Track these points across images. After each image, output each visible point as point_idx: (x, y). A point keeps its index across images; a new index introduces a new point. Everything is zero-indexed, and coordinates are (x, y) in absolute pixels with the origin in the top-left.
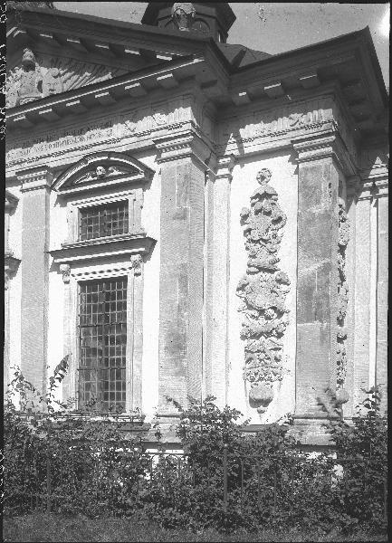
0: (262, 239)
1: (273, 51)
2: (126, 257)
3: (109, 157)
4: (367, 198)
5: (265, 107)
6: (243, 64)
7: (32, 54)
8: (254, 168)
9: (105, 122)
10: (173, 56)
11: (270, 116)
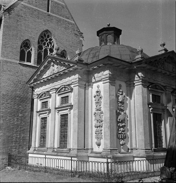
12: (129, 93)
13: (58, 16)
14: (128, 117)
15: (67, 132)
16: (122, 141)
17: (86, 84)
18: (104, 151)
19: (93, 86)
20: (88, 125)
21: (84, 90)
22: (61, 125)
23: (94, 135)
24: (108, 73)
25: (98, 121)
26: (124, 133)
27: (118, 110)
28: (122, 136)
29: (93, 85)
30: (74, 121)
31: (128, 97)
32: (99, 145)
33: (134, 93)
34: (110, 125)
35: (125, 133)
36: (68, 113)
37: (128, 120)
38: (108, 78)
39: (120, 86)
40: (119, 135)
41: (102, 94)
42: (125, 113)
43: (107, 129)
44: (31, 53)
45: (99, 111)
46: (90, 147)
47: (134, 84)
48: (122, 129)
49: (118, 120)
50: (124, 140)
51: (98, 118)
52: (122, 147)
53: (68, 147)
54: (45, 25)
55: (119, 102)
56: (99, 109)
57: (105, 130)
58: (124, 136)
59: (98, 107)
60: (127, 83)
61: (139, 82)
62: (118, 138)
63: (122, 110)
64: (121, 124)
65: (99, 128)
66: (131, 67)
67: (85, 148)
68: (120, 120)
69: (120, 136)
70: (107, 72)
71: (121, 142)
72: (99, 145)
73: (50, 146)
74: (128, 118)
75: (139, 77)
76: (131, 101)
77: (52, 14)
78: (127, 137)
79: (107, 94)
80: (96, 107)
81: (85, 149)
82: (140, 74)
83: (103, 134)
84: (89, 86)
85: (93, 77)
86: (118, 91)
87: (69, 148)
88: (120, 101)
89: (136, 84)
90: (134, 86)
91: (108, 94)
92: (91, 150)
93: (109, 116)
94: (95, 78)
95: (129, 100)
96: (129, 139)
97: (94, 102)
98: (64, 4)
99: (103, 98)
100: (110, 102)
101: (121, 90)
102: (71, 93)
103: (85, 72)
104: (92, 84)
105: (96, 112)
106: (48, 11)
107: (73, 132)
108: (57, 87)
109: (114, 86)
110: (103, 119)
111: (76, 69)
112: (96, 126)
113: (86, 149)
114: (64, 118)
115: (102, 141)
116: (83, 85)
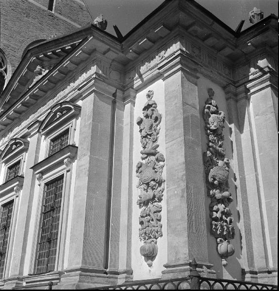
0: (148, 134)
1: (49, 39)
2: (61, 163)
3: (61, 106)
4: (243, 98)
5: (146, 55)
6: (243, 29)
7: (211, 128)
8: (145, 92)
9: (62, 88)
10: (71, 46)
11: (150, 58)
12: (234, 113)
13: (69, 21)
14: (237, 177)
15: (57, 227)
16: (225, 243)
17: (118, 94)
18: (168, 272)
19: (137, 100)
20: (120, 201)
21: (110, 107)
22: (45, 210)
23: (136, 227)
24: (178, 47)
25: (148, 184)
26: (228, 220)
27: (208, 152)
28: (222, 227)
29: (135, 97)
30: (78, 189)
31: (232, 126)
32: (150, 256)
33: (249, 114)
34: (187, 186)
35: (231, 221)
36: (65, 172)
37: (236, 188)
38: (178, 59)
39: (211, 93)
40: (214, 222)
41: (161, 109)
42: (227, 164)
43: (178, 199)
44: (4, 77)
45: (153, 158)
46: (122, 267)
47: (248, 90)
48: (221, 207)
49: (211, 180)
50: (229, 242)
51: (148, 174)
52: (224, 262)
53: (55, 270)
54: (42, 30)
55: (211, 130)
56: (153, 151)
57: (172, 204)
58: (228, 228)
59: (149, 148)
60: (227, 89)
61: (261, 83)
62: (212, 233)
63: (221, 156)
64: (218, 191)
65: (150, 205)
66: (236, 47)
67: (106, 267)
68: (215, 179)
69: (216, 225)
70: (175, 48)
71: (223, 247)
72: (150, 256)
73: (13, 274)
74: (235, 179)
75: (261, 69)
76: (242, 136)
77: (56, 14)
78: (237, 236)
79: (176, 101)
80: (142, 149)
81: (106, 273)
82: (262, 63)
83: (164, 222)
84: (124, 99)
85: (137, 76)
86: (206, 103)
87: (60, 269)
88: (213, 127)
89: (252, 91)
90: (248, 99)
91: (179, 101)
92: (125, 275)
93: (182, 159)
94: (140, 76)
95: (235, 131)
96: (244, 240)
97: (137, 136)
98: (83, 4)
99: (163, 119)
100: (186, 120)
101: (213, 102)
102: (77, 119)
103: (115, 63)
104: (132, 94)
105: (144, 162)
106: (50, 8)
107: (73, 219)
108: (41, 119)
109: (196, 85)
110: (164, 176)
111: (91, 52)
112: (143, 200)
113: (111, 273)
114: (55, 187)
115: (162, 244)
116: (109, 93)
